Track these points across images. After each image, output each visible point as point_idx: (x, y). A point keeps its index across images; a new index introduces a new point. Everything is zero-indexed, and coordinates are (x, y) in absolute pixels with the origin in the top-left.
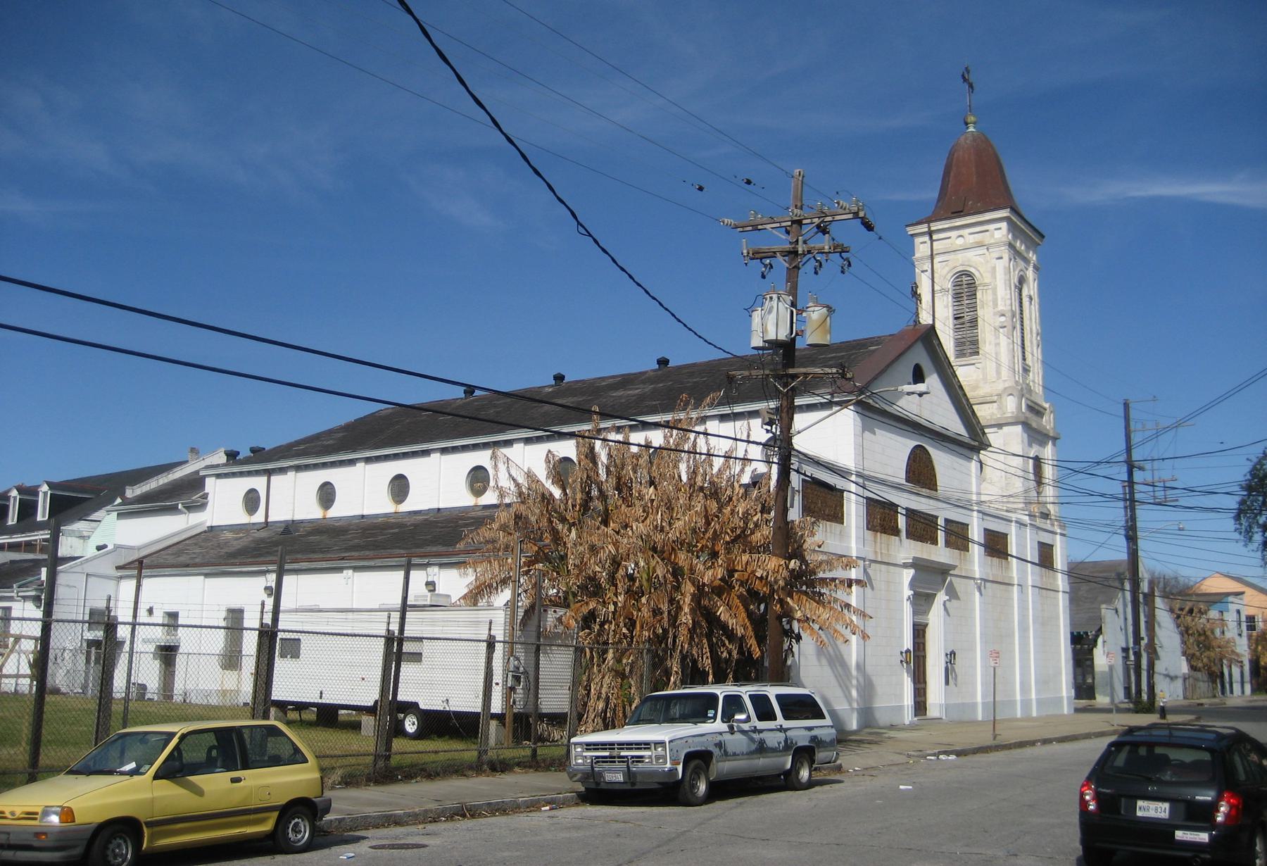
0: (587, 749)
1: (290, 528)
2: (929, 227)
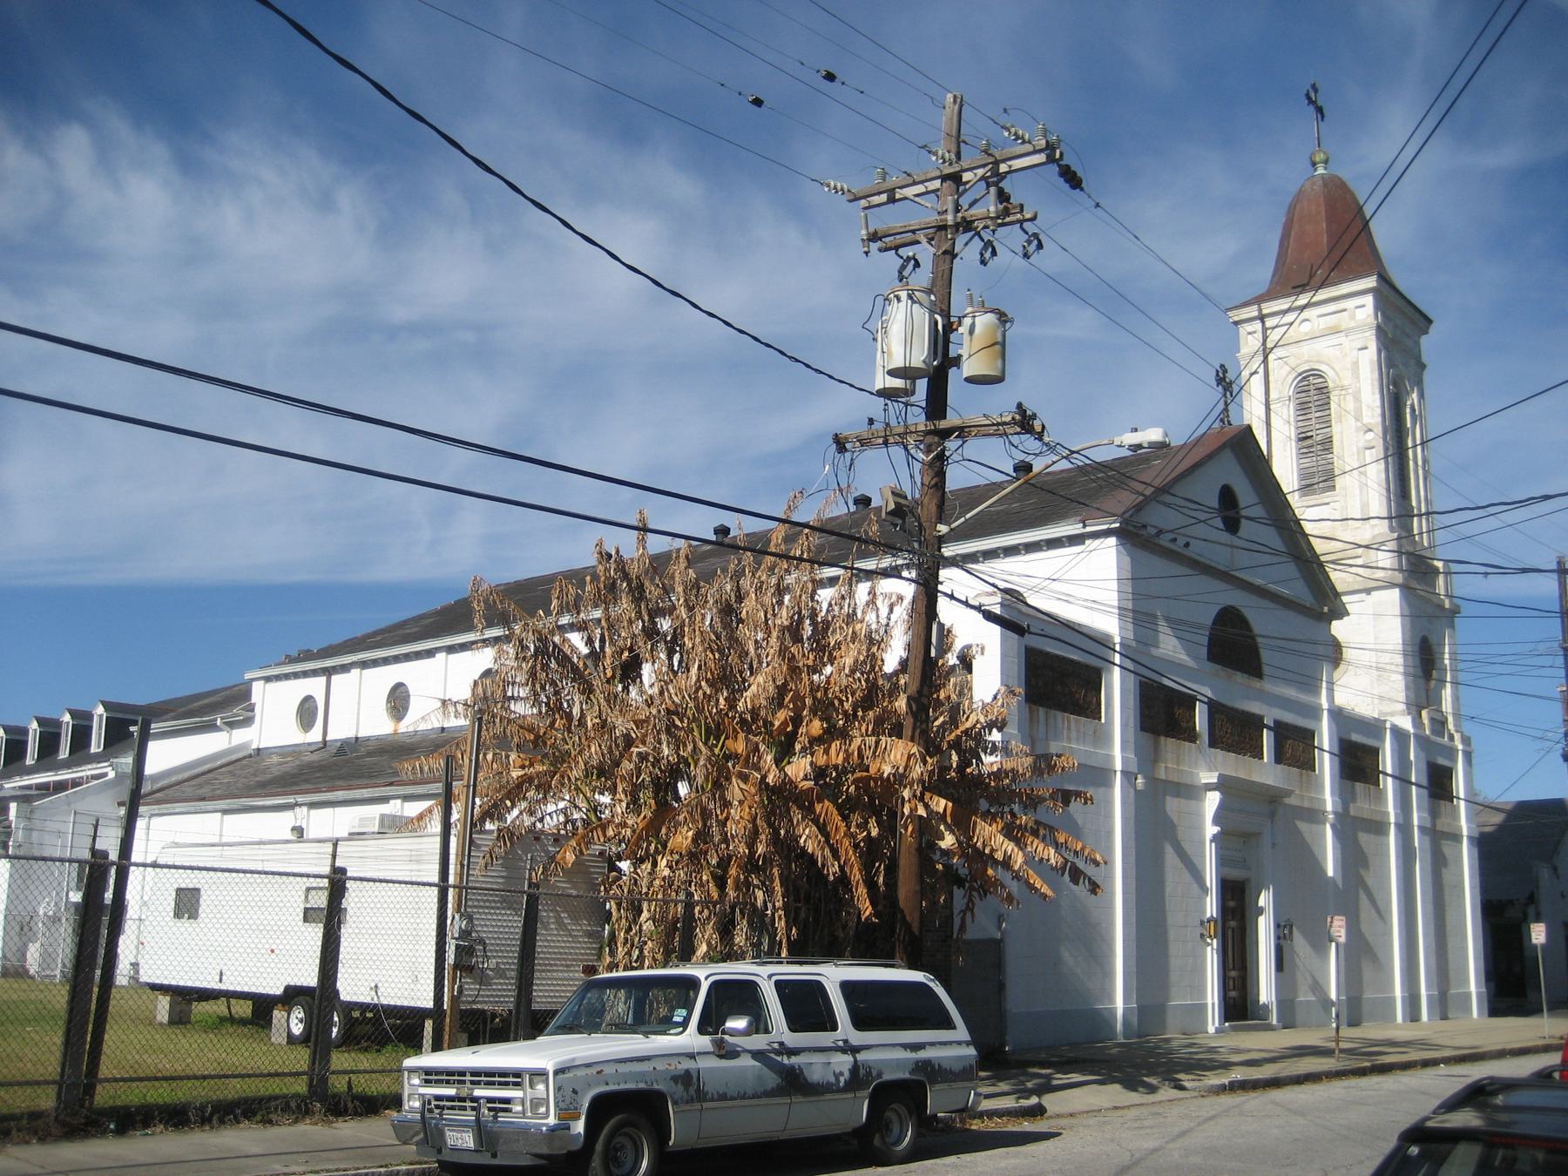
0: (427, 1081)
1: (351, 747)
2: (1260, 310)
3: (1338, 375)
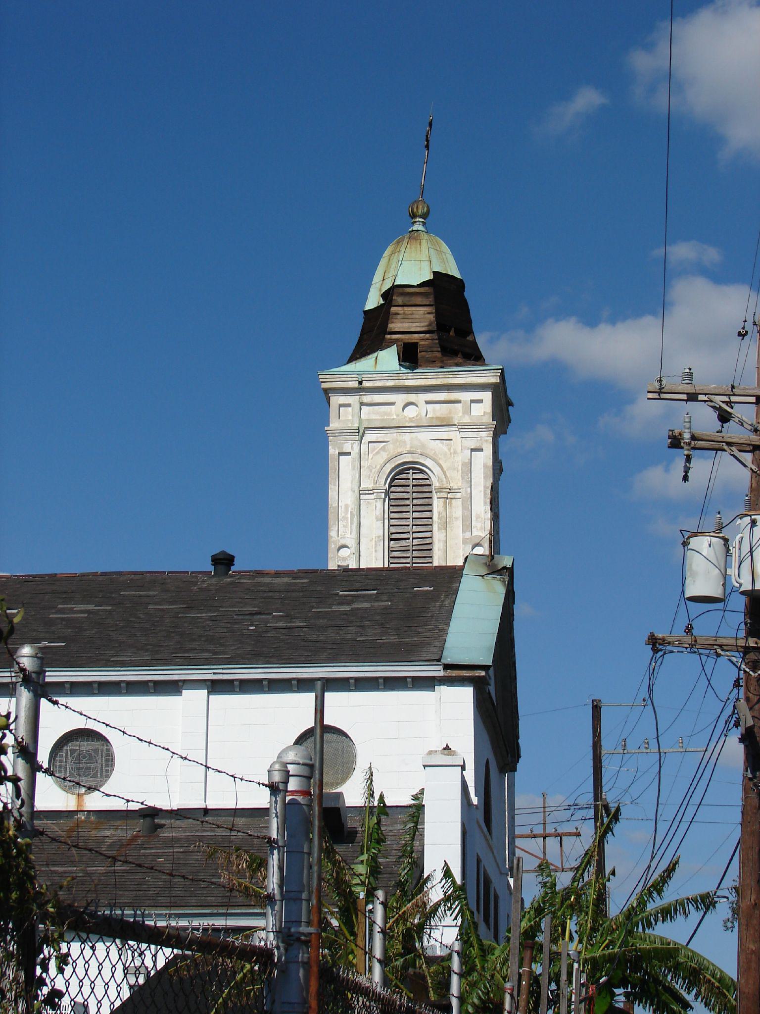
3: (444, 473)
